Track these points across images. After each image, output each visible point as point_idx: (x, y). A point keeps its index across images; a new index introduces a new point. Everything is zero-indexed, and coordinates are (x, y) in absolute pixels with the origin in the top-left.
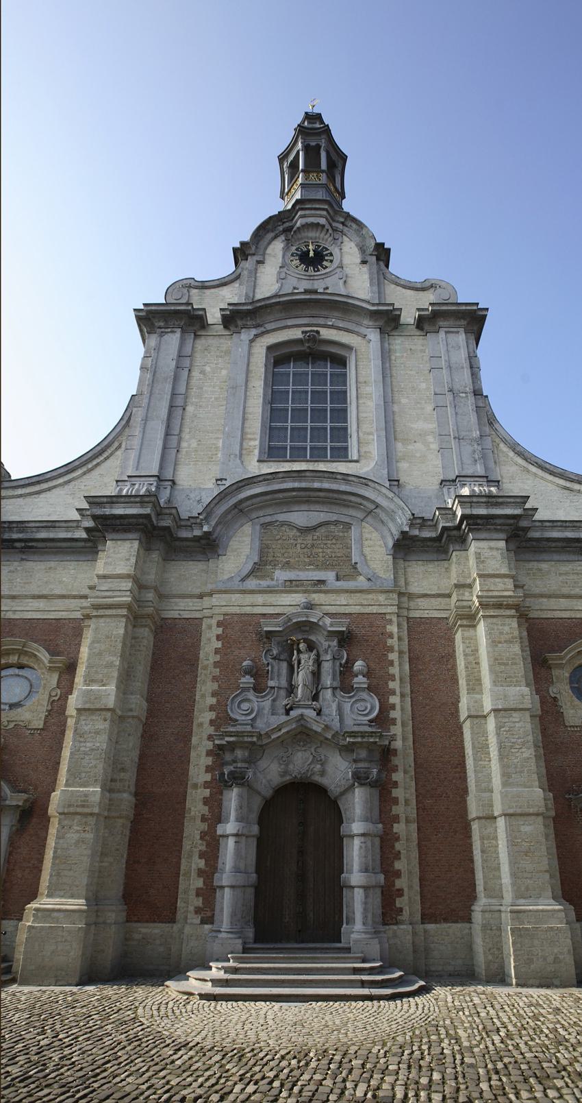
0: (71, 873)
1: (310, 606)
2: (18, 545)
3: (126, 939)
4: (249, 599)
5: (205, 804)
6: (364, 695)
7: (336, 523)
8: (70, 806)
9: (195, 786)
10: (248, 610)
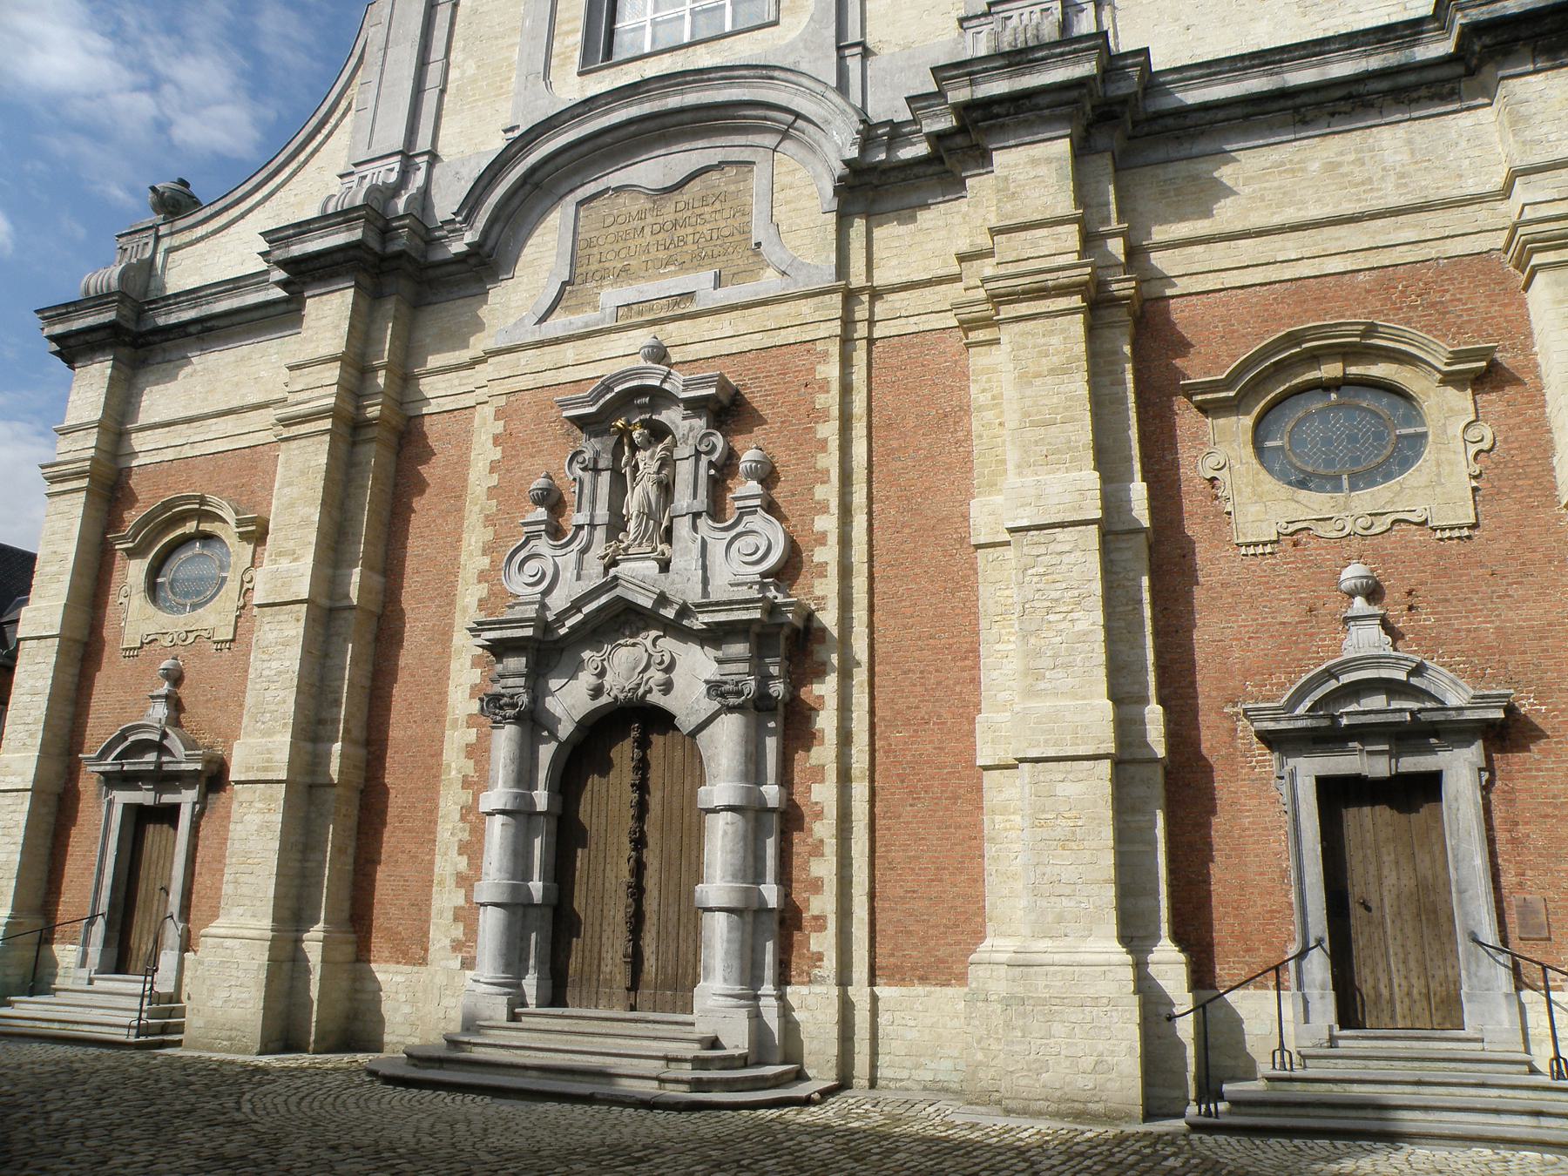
0: (251, 879)
1: (659, 354)
2: (192, 329)
3: (356, 991)
4: (550, 355)
5: (469, 755)
7: (721, 165)
8: (248, 769)
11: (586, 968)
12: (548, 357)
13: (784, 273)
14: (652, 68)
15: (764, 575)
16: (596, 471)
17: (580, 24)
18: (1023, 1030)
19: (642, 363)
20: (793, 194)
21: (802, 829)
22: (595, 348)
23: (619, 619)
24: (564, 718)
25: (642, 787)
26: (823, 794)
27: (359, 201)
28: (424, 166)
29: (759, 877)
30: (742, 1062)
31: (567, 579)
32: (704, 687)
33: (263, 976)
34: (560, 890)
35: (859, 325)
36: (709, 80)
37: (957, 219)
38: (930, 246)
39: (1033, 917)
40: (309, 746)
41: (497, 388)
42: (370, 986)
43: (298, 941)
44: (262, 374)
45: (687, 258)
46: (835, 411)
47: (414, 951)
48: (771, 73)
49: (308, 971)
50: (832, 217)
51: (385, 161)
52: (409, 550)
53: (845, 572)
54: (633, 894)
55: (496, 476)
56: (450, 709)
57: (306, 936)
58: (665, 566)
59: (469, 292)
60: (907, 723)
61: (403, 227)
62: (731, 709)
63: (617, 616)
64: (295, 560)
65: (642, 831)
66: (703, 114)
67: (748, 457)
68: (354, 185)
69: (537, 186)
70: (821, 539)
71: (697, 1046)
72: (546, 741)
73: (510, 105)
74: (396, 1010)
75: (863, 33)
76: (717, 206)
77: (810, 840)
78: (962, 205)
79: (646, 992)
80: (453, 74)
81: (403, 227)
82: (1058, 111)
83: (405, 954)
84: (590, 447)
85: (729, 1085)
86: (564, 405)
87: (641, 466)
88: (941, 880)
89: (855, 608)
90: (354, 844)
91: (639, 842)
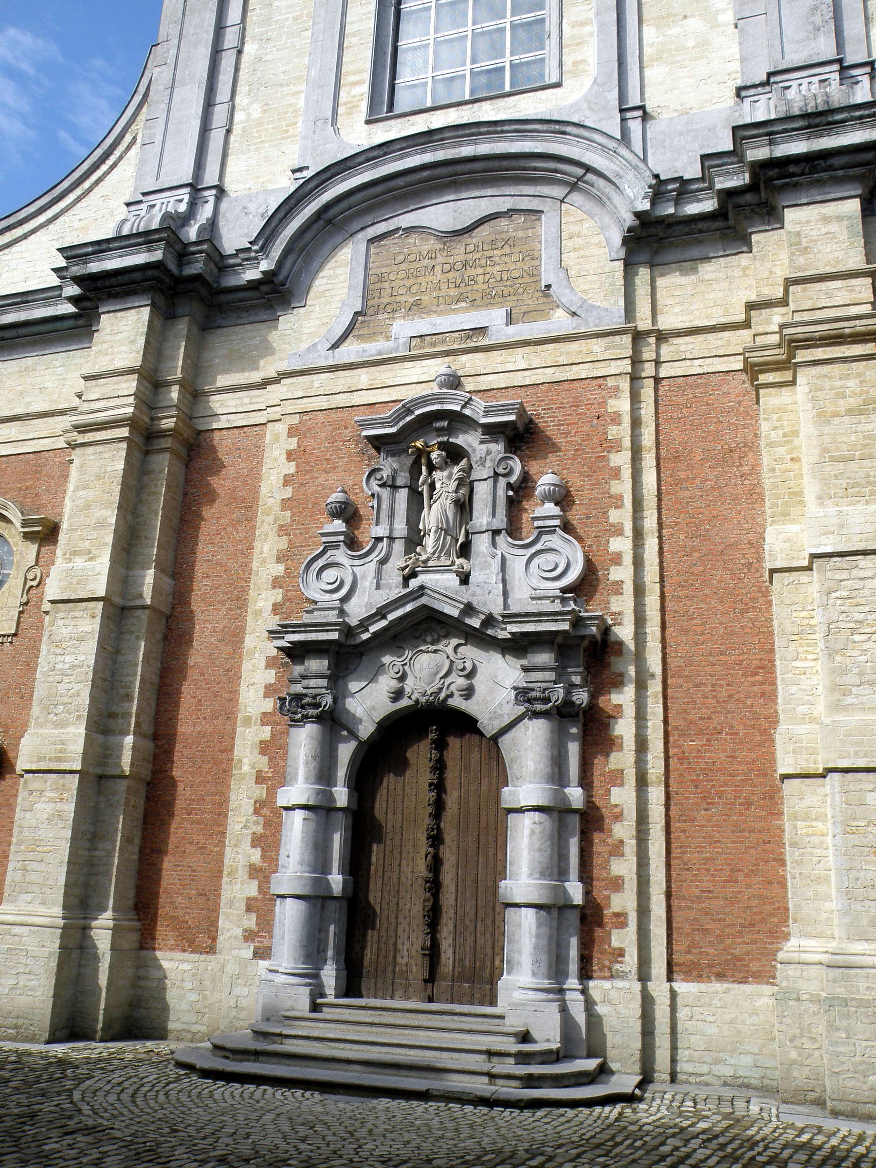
1: (454, 382)
4: (344, 379)
5: (263, 752)
6: (555, 540)
7: (510, 213)
8: (40, 759)
9: (248, 721)
10: (342, 400)
11: (381, 960)
12: (341, 381)
13: (574, 314)
14: (438, 120)
15: (564, 590)
16: (394, 487)
17: (367, 76)
18: (847, 1032)
19: (437, 390)
20: (582, 245)
21: (602, 830)
22: (389, 374)
23: (423, 625)
24: (365, 718)
25: (439, 787)
26: (623, 796)
27: (155, 224)
28: (212, 200)
29: (562, 874)
30: (554, 1057)
31: (368, 590)
32: (513, 693)
33: (54, 964)
34: (356, 884)
35: (647, 365)
36: (503, 132)
37: (737, 273)
38: (711, 296)
39: (847, 920)
40: (100, 738)
41: (290, 407)
42: (155, 974)
43: (86, 929)
44: (47, 384)
45: (478, 296)
46: (627, 442)
47: (202, 938)
48: (564, 128)
49: (96, 959)
50: (620, 265)
51: (174, 192)
52: (199, 556)
53: (639, 591)
54: (430, 889)
55: (289, 489)
56: (241, 707)
57: (94, 923)
58: (465, 579)
59: (258, 318)
60: (700, 733)
61: (201, 252)
62: (536, 715)
63: (419, 623)
64: (91, 559)
65: (439, 829)
66: (496, 164)
67: (545, 481)
68: (143, 213)
69: (329, 222)
70: (617, 559)
71: (512, 1039)
72: (345, 740)
73: (297, 147)
74: (181, 997)
75: (642, 99)
76: (507, 250)
77: (610, 841)
78: (744, 260)
79: (444, 983)
80: (238, 117)
81: (201, 252)
82: (851, 172)
83: (191, 942)
84: (388, 465)
85: (559, 1081)
86: (364, 425)
87: (438, 485)
88: (736, 881)
89: (648, 624)
90: (140, 834)
91: (436, 839)
